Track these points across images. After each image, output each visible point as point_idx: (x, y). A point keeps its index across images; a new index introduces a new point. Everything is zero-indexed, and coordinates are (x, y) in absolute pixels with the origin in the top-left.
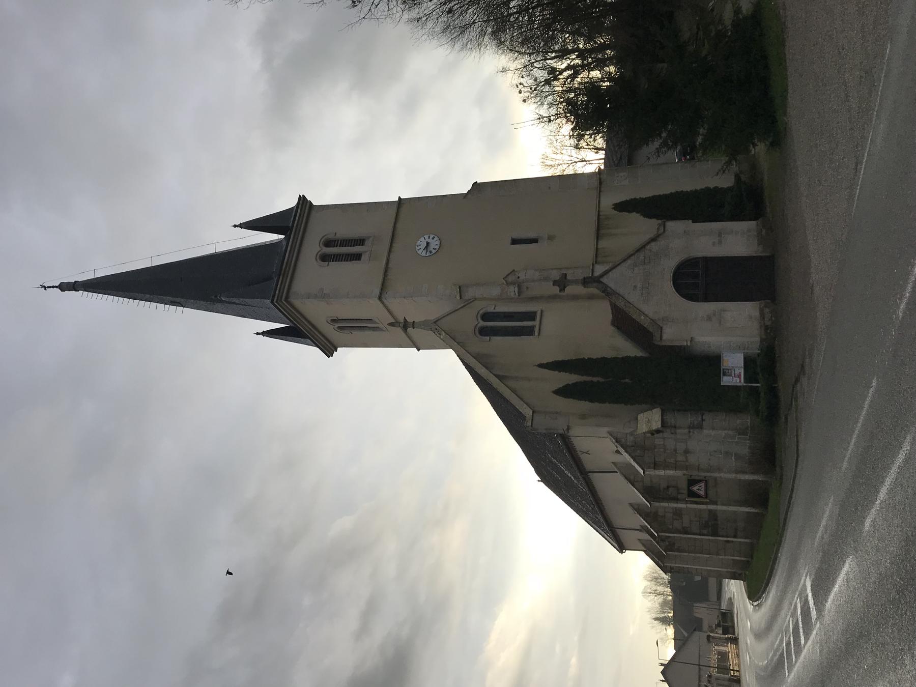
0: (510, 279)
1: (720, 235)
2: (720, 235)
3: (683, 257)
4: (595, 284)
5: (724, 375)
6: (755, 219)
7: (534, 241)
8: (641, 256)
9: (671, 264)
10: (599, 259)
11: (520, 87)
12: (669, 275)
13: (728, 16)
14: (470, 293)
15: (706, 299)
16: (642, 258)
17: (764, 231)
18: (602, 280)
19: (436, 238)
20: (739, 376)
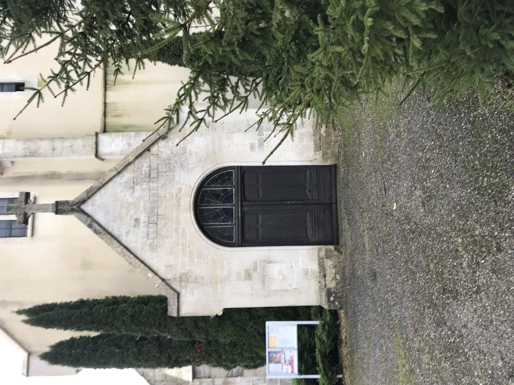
4: (77, 214)
5: (270, 362)
8: (144, 164)
9: (190, 180)
10: (109, 120)
12: (188, 201)
16: (145, 169)
18: (84, 207)
20: (291, 363)
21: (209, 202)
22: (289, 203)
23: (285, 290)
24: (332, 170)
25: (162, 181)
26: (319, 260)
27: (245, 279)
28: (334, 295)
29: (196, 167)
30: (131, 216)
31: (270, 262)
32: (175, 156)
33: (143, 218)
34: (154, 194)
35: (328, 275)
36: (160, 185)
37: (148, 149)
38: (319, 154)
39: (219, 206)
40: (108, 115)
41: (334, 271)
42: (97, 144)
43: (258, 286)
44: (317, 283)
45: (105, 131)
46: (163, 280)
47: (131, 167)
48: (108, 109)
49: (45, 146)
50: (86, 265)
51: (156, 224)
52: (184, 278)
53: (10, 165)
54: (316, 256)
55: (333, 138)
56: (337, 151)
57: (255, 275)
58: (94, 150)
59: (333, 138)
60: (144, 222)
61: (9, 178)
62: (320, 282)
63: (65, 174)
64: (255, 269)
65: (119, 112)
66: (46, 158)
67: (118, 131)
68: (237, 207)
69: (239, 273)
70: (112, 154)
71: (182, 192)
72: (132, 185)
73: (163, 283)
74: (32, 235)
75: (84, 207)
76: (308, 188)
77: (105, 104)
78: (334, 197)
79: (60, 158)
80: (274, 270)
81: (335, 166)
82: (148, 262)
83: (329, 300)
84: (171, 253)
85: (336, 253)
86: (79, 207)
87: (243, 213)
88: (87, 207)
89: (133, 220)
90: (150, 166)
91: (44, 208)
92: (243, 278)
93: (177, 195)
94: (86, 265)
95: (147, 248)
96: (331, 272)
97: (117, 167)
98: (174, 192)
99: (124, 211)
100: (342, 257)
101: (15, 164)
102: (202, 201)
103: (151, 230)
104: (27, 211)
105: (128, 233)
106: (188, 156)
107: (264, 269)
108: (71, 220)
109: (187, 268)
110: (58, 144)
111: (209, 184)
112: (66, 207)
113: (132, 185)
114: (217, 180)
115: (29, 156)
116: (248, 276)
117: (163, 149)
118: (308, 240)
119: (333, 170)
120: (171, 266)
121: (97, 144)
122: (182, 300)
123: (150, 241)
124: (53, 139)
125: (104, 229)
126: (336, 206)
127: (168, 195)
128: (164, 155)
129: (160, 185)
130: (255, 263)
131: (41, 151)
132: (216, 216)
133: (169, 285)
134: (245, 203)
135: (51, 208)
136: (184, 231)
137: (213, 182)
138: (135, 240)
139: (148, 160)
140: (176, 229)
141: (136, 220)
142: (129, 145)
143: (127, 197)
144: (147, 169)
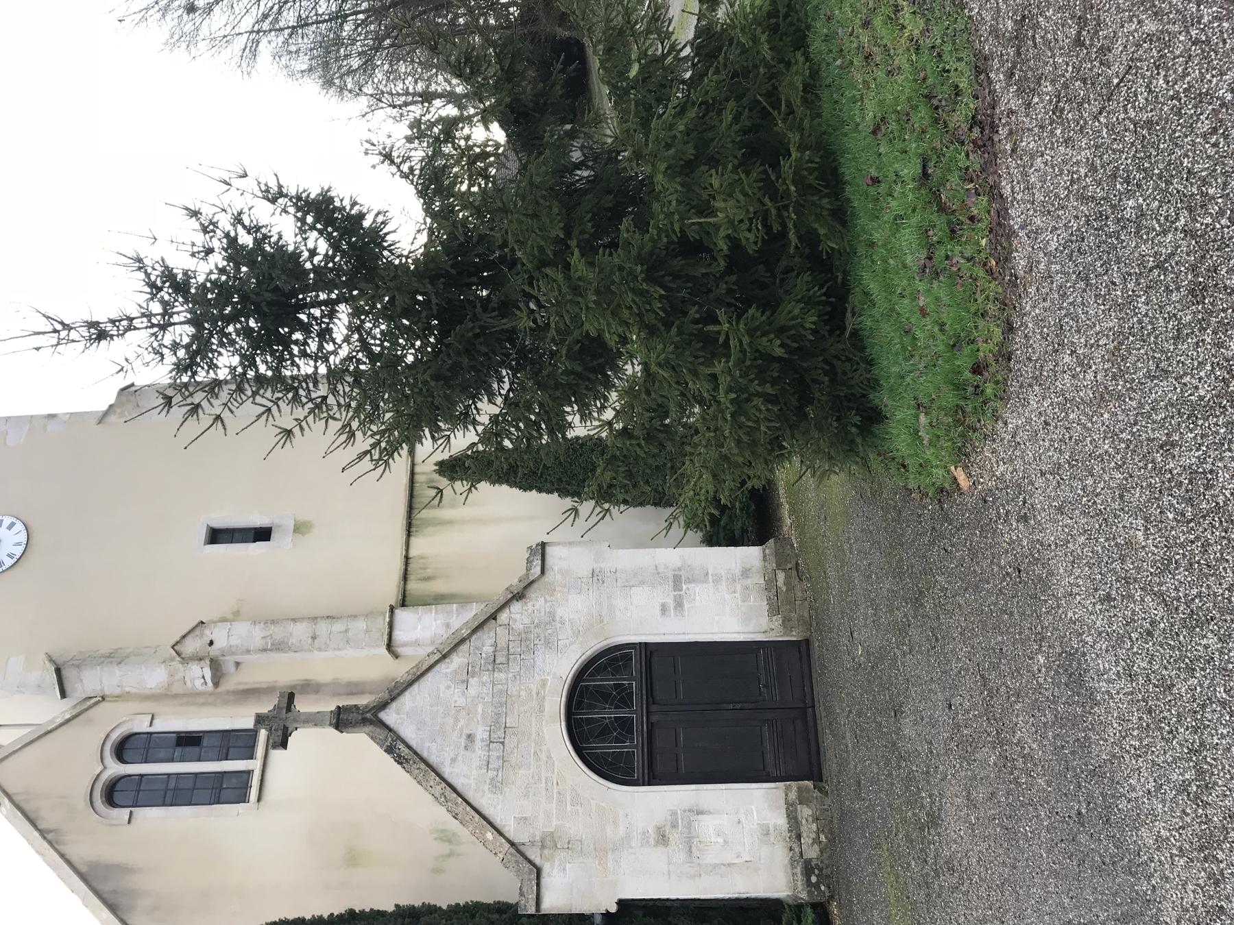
0: (190, 646)
1: (677, 581)
2: (677, 581)
3: (595, 645)
4: (370, 728)
6: (760, 541)
7: (263, 534)
8: (485, 642)
9: (559, 668)
10: (413, 586)
11: (368, 146)
12: (556, 702)
13: (684, 30)
14: (88, 682)
15: (653, 778)
17: (781, 576)
18: (383, 716)
19: (19, 526)
21: (591, 707)
22: (731, 706)
23: (729, 865)
24: (802, 648)
25: (514, 668)
26: (787, 809)
27: (657, 843)
28: (817, 872)
29: (571, 644)
30: (461, 730)
31: (700, 813)
32: (537, 626)
33: (481, 733)
34: (501, 691)
35: (804, 835)
36: (511, 675)
37: (493, 617)
38: (777, 622)
39: (609, 714)
40: (411, 577)
41: (814, 827)
42: (391, 625)
43: (681, 856)
44: (786, 851)
45: (403, 604)
46: (512, 844)
47: (464, 647)
48: (412, 567)
49: (300, 631)
50: (353, 859)
51: (503, 743)
52: (548, 842)
53: (232, 668)
54: (782, 802)
55: (799, 594)
56: (806, 615)
57: (674, 837)
58: (386, 637)
59: (799, 594)
60: (482, 740)
61: (228, 692)
62: (791, 849)
63: (327, 685)
64: (674, 826)
65: (429, 572)
66: (297, 655)
67: (426, 603)
68: (642, 713)
69: (645, 833)
70: (417, 643)
71: (548, 687)
72: (465, 677)
73: (512, 850)
74: (259, 800)
75: (383, 716)
76: (763, 681)
77: (407, 558)
78: (808, 697)
79: (323, 655)
80: (707, 826)
81: (807, 642)
82: (486, 812)
83: (809, 880)
84: (527, 796)
85: (817, 794)
86: (375, 715)
87: (651, 726)
88: (389, 716)
89: (464, 737)
90: (495, 645)
91: (314, 720)
92: (652, 841)
93: (538, 694)
94: (353, 859)
95: (486, 787)
96: (809, 830)
97: (441, 648)
98: (534, 688)
99: (450, 721)
100: (828, 801)
101: (242, 666)
102: (579, 704)
103: (494, 754)
104: (288, 725)
105: (454, 760)
106: (559, 625)
107: (689, 825)
108: (360, 741)
109: (555, 822)
110: (323, 628)
111: (592, 675)
112: (354, 716)
113: (465, 677)
114: (606, 668)
115: (271, 650)
116: (663, 838)
117: (518, 616)
118: (768, 775)
119: (803, 648)
120: (525, 819)
121: (391, 625)
122: (545, 881)
123: (491, 774)
124: (314, 619)
125: (416, 753)
126: (814, 712)
127: (523, 693)
128: (518, 626)
129: (511, 675)
130: (674, 814)
131: (293, 641)
132: (604, 732)
133: (519, 851)
134: (654, 708)
135: (328, 718)
136: (549, 757)
137: (598, 670)
138: (465, 772)
139: (492, 634)
140: (535, 753)
141: (469, 736)
142: (448, 626)
143: (456, 697)
144: (491, 649)
